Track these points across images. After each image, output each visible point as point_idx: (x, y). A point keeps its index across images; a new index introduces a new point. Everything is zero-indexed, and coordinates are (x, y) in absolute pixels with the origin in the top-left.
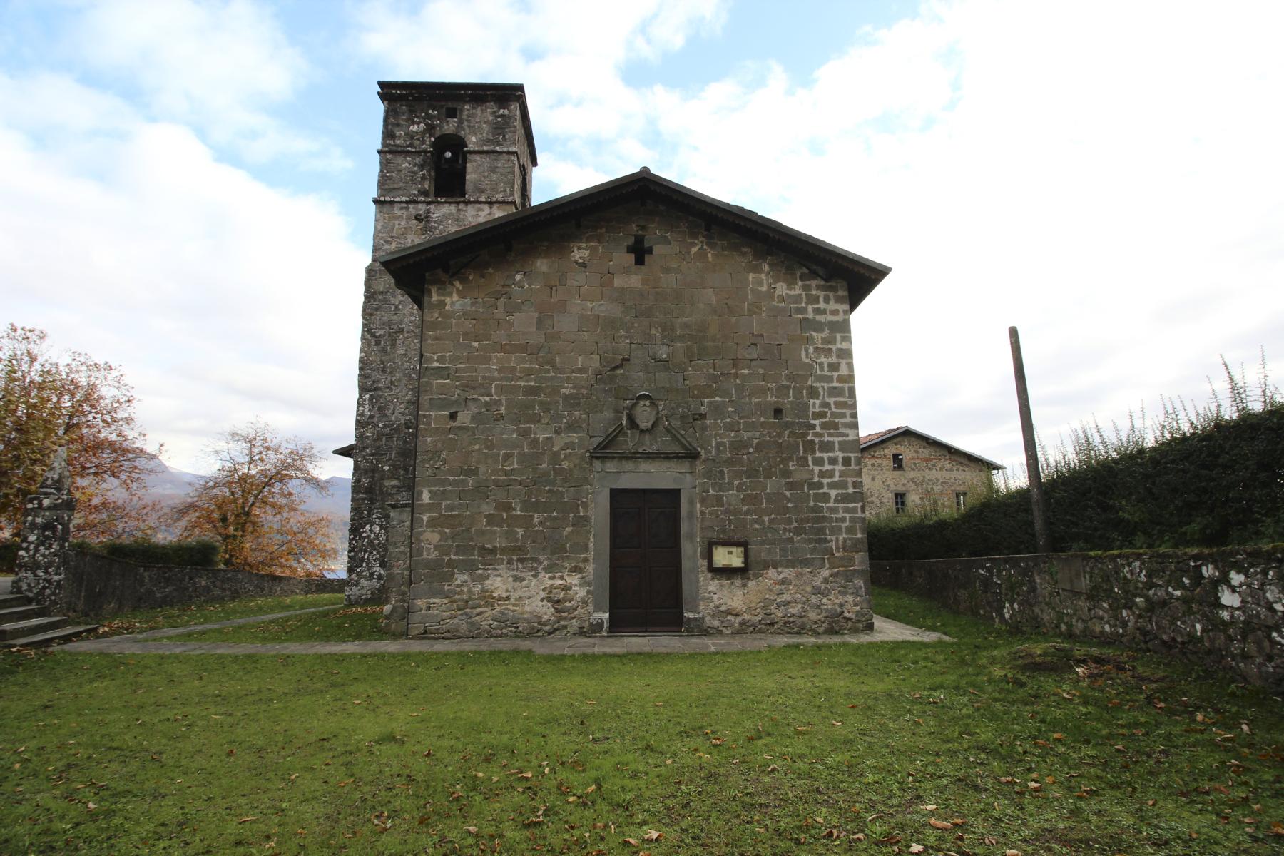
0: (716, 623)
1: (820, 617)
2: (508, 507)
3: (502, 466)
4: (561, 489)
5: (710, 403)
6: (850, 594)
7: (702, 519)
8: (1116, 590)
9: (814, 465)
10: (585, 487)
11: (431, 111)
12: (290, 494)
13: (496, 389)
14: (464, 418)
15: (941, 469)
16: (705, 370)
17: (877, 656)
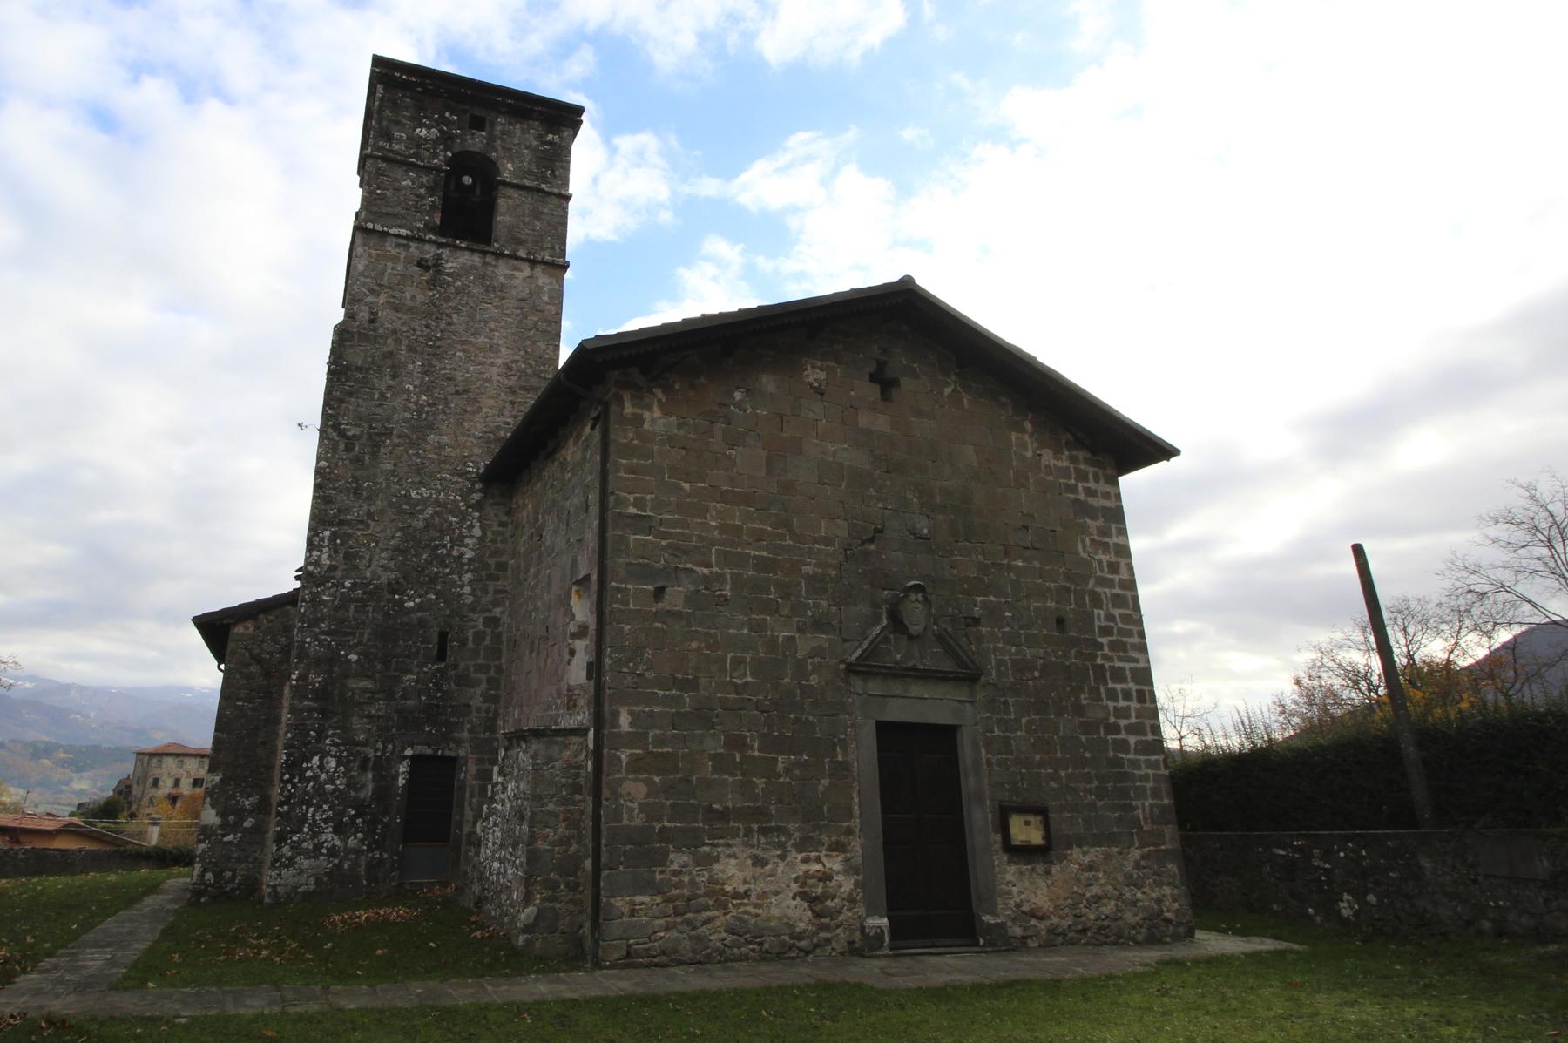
3: (731, 677)
4: (811, 718)
5: (984, 603)
9: (1107, 699)
10: (842, 717)
11: (447, 114)
14: (676, 597)
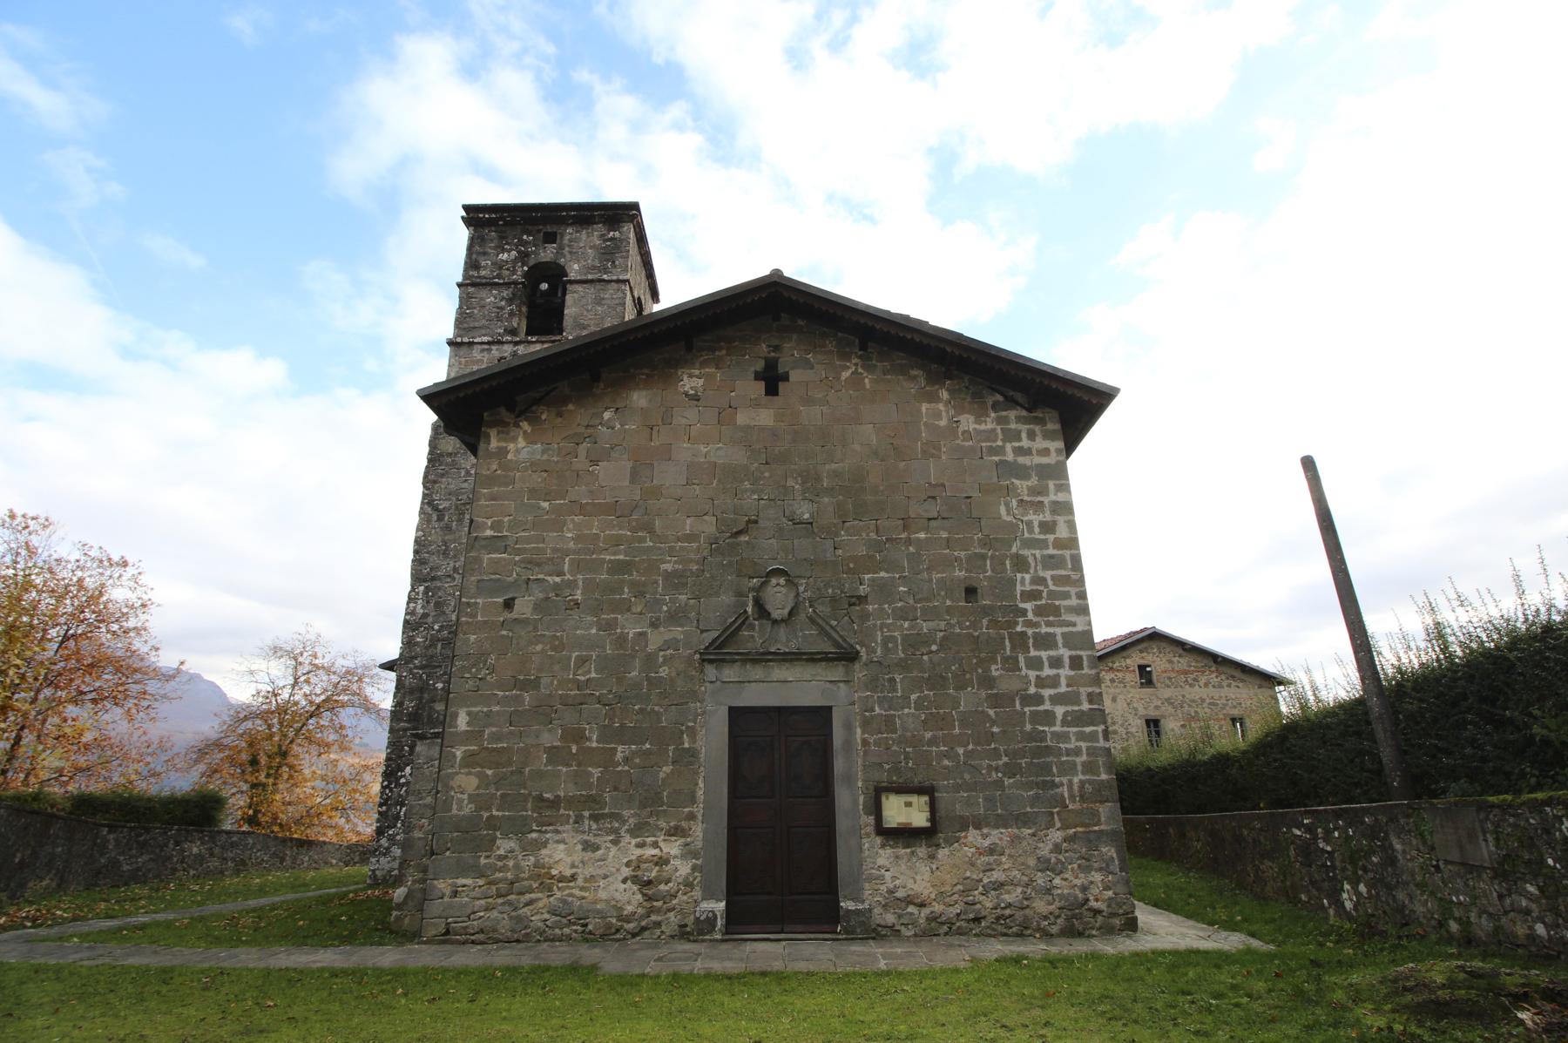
0: (890, 918)
1: (1052, 908)
2: (579, 736)
3: (574, 674)
4: (656, 708)
5: (873, 580)
6: (1096, 870)
7: (865, 753)
8: (1550, 862)
11: (525, 237)
12: (342, 727)
13: (570, 565)
14: (524, 607)
15: (1206, 685)
16: (864, 535)
17: (1149, 980)
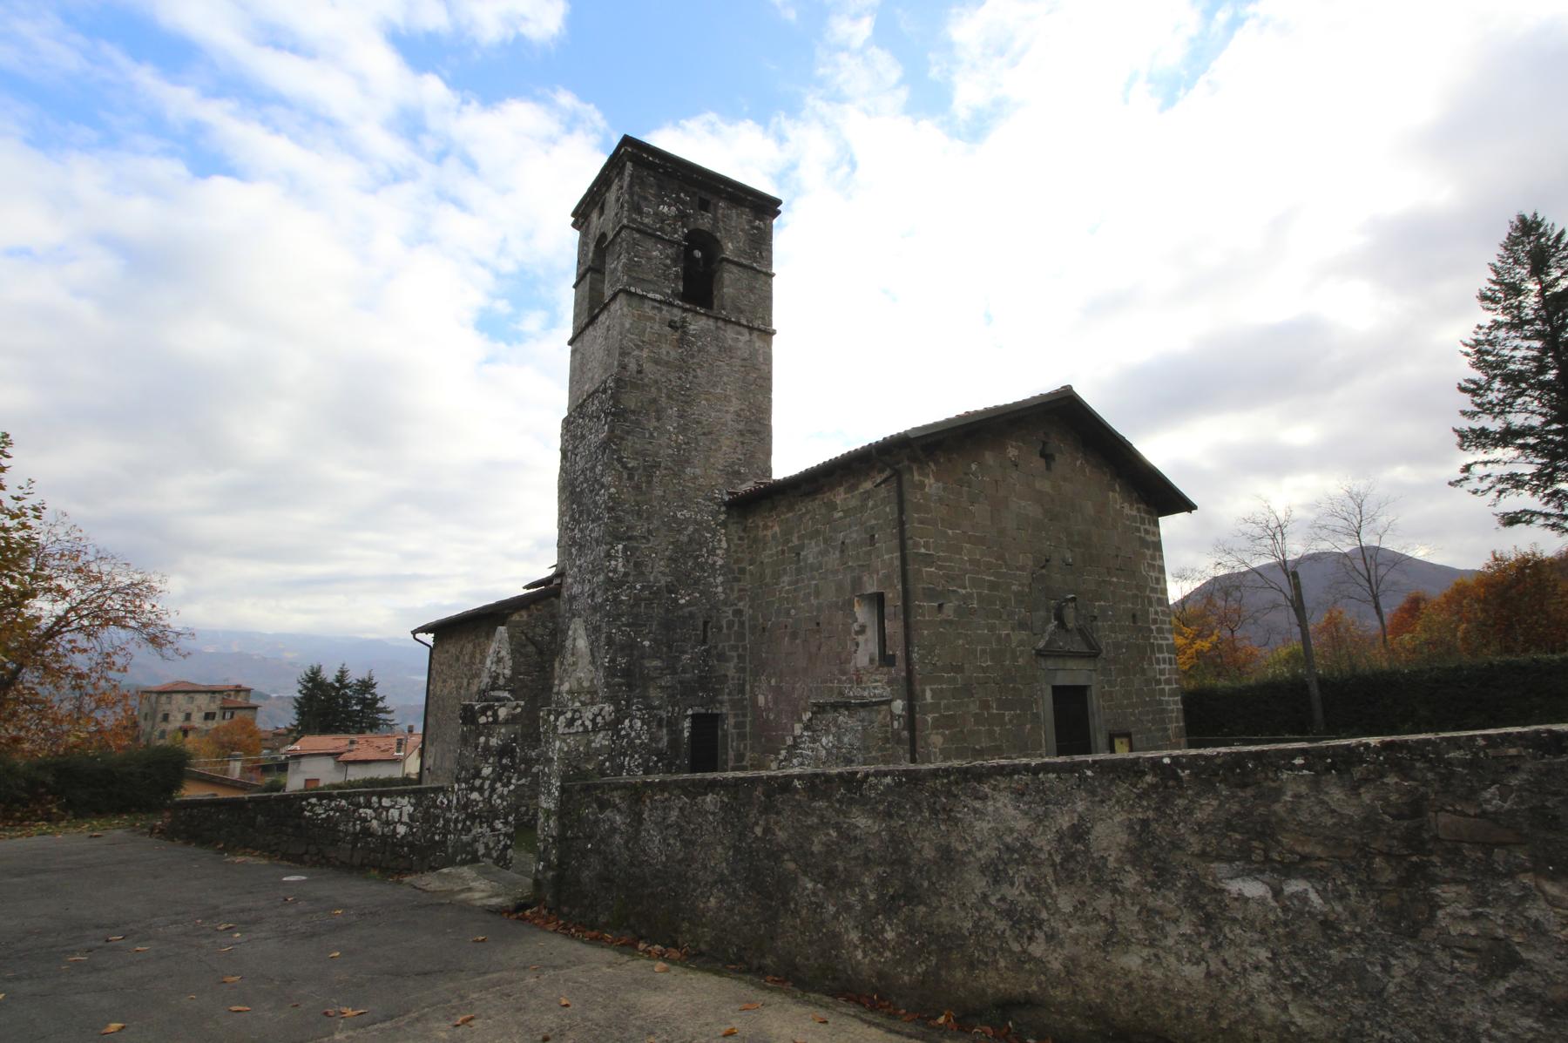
11: (682, 195)
14: (949, 608)
